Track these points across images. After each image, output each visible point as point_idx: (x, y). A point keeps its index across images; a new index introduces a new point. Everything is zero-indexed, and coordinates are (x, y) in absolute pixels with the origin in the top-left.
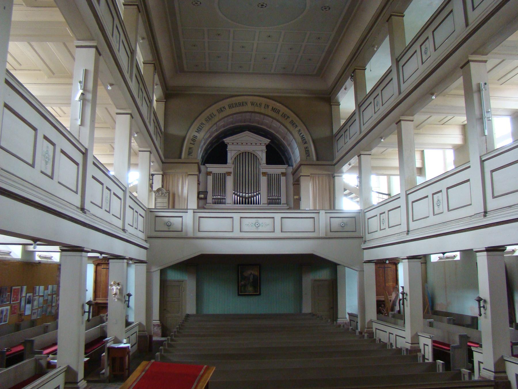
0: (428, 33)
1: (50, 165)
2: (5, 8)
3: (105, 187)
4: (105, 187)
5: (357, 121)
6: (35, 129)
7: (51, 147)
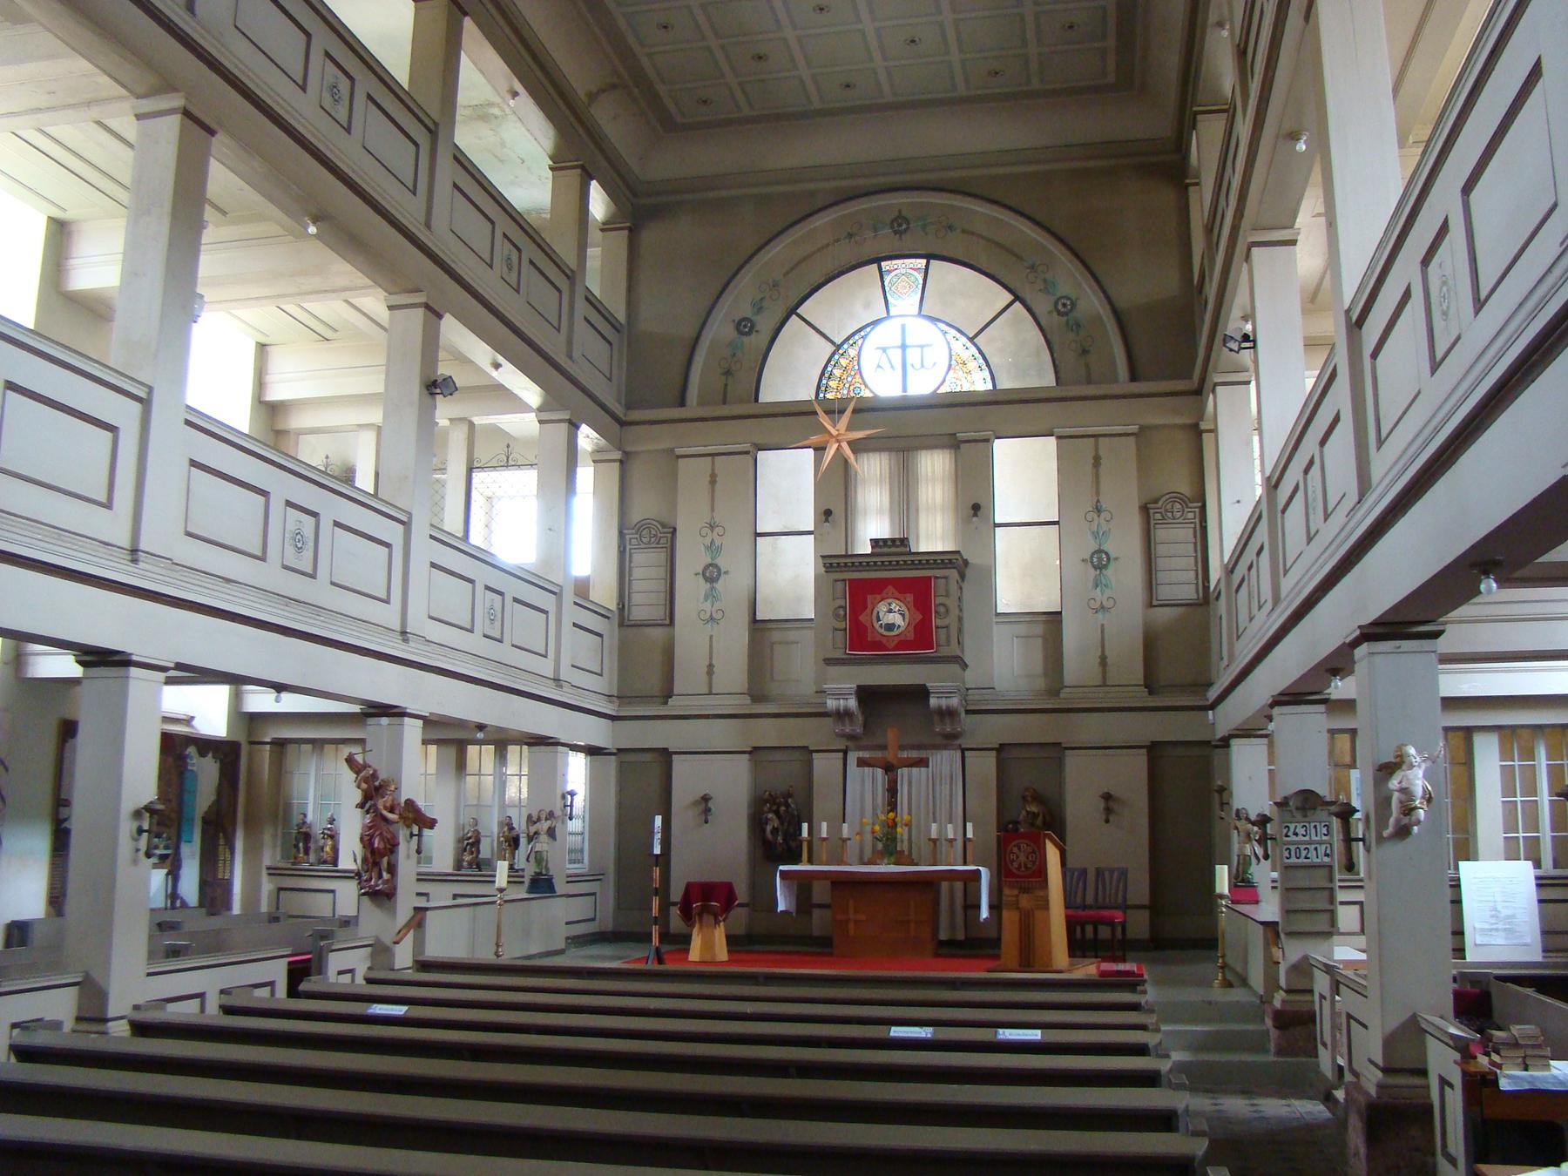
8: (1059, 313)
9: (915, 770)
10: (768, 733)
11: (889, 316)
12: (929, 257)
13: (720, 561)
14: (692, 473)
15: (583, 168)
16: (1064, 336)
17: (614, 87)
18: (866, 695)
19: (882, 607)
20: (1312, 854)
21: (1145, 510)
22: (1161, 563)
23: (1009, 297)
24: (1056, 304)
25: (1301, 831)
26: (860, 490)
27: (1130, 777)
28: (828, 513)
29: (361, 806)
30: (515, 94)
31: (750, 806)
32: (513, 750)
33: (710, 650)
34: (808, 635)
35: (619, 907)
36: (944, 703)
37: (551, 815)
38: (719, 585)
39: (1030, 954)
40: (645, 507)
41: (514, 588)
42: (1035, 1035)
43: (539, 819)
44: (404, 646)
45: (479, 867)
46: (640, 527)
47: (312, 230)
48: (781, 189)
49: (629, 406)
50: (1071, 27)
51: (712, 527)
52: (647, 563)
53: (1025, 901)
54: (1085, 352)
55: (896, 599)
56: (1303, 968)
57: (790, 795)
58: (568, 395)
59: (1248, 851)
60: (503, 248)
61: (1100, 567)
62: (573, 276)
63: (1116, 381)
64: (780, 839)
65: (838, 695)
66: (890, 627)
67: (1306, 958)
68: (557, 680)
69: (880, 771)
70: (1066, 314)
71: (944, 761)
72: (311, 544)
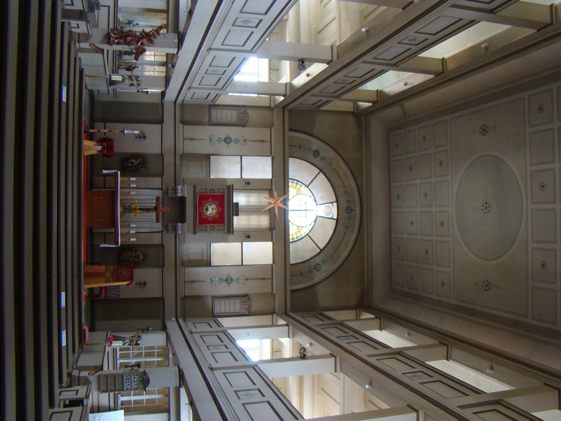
0: (437, 377)
1: (242, 24)
2: (442, 224)
3: (221, 76)
4: (221, 76)
5: (322, 322)
6: (266, 13)
7: (255, 25)
8: (315, 266)
9: (155, 218)
10: (169, 161)
11: (317, 205)
12: (337, 220)
13: (232, 143)
14: (264, 133)
15: (377, 102)
16: (307, 267)
17: (405, 114)
18: (182, 200)
19: (214, 206)
20: (127, 384)
21: (246, 295)
22: (227, 301)
23: (322, 247)
24: (318, 264)
25: (135, 380)
26: (255, 194)
27: (152, 291)
28: (248, 183)
29: (143, 31)
30: (406, 84)
31: (142, 154)
32: (164, 69)
33: (200, 139)
34: (203, 175)
35: (104, 103)
36: (179, 228)
37: (139, 85)
38: (223, 143)
39: (90, 276)
40: (253, 115)
41: (224, 79)
42: (64, 343)
43: (137, 81)
44: (206, 49)
45: (119, 55)
46: (246, 114)
47: (364, 30)
48: (364, 170)
49: (290, 111)
50: (412, 278)
51: (245, 141)
52: (232, 116)
53: (108, 274)
54: (301, 274)
55: (217, 210)
56: (87, 382)
57: (146, 168)
58: (295, 95)
59: (126, 341)
60: (351, 80)
61: (226, 280)
62: (338, 97)
63: (291, 285)
64: (129, 165)
65: (182, 190)
66: (207, 209)
67: (91, 383)
68: (190, 88)
69: (154, 205)
70: (315, 267)
71: (158, 226)
72: (245, 25)
